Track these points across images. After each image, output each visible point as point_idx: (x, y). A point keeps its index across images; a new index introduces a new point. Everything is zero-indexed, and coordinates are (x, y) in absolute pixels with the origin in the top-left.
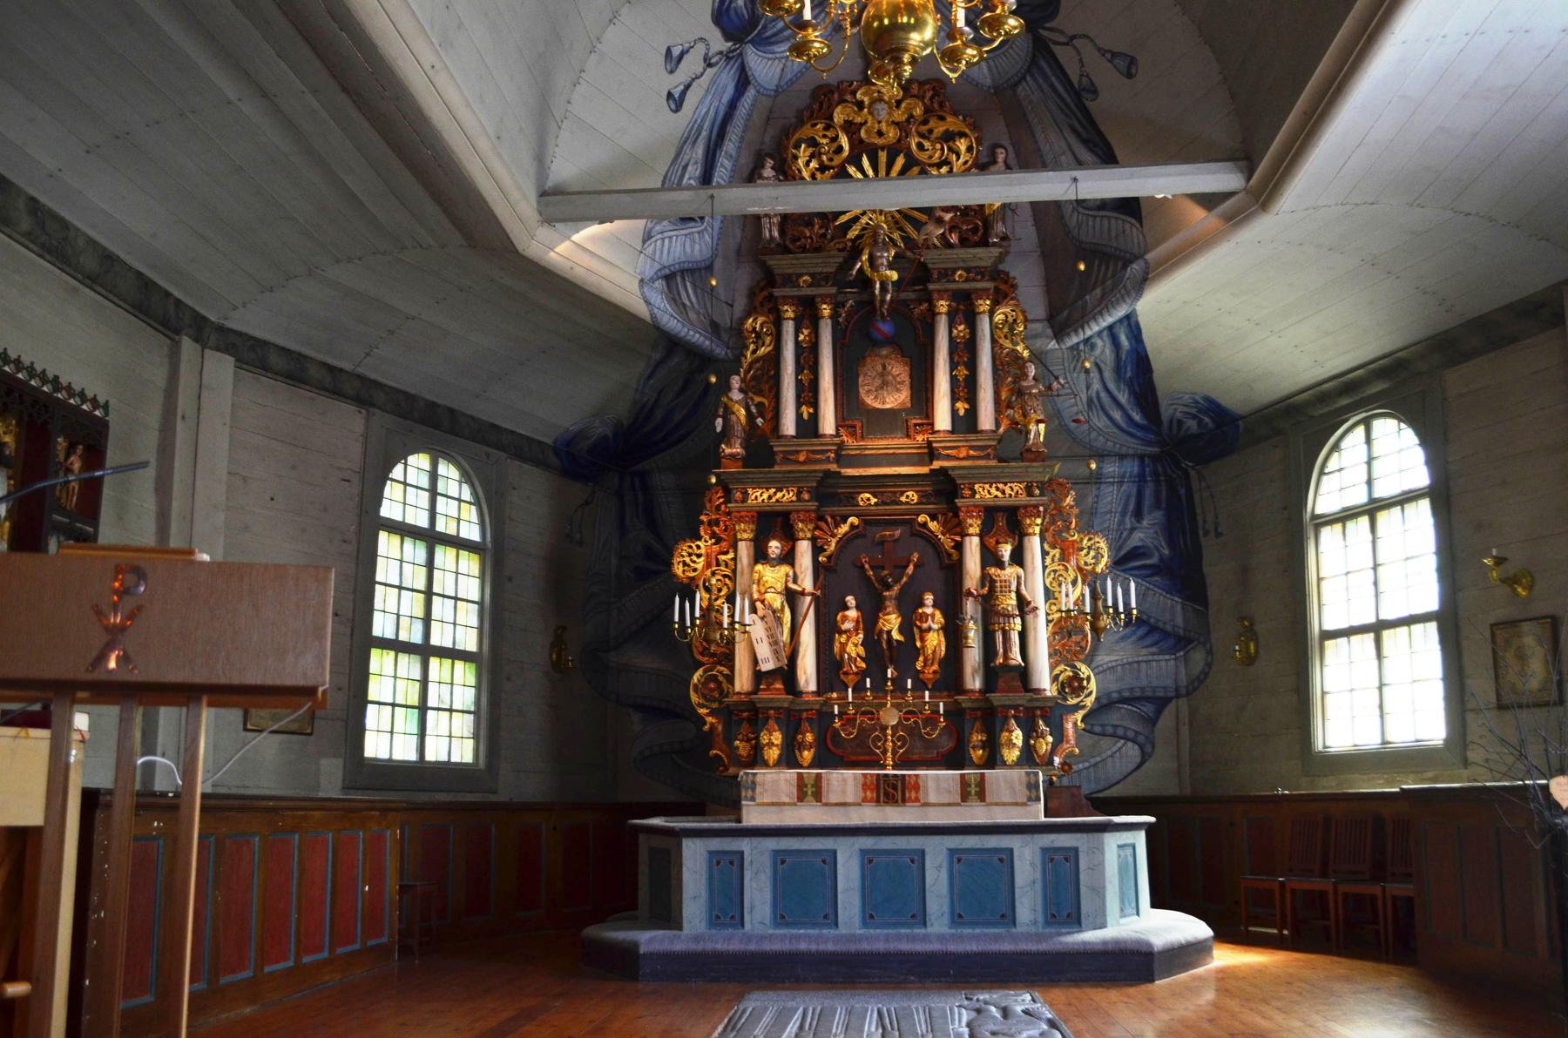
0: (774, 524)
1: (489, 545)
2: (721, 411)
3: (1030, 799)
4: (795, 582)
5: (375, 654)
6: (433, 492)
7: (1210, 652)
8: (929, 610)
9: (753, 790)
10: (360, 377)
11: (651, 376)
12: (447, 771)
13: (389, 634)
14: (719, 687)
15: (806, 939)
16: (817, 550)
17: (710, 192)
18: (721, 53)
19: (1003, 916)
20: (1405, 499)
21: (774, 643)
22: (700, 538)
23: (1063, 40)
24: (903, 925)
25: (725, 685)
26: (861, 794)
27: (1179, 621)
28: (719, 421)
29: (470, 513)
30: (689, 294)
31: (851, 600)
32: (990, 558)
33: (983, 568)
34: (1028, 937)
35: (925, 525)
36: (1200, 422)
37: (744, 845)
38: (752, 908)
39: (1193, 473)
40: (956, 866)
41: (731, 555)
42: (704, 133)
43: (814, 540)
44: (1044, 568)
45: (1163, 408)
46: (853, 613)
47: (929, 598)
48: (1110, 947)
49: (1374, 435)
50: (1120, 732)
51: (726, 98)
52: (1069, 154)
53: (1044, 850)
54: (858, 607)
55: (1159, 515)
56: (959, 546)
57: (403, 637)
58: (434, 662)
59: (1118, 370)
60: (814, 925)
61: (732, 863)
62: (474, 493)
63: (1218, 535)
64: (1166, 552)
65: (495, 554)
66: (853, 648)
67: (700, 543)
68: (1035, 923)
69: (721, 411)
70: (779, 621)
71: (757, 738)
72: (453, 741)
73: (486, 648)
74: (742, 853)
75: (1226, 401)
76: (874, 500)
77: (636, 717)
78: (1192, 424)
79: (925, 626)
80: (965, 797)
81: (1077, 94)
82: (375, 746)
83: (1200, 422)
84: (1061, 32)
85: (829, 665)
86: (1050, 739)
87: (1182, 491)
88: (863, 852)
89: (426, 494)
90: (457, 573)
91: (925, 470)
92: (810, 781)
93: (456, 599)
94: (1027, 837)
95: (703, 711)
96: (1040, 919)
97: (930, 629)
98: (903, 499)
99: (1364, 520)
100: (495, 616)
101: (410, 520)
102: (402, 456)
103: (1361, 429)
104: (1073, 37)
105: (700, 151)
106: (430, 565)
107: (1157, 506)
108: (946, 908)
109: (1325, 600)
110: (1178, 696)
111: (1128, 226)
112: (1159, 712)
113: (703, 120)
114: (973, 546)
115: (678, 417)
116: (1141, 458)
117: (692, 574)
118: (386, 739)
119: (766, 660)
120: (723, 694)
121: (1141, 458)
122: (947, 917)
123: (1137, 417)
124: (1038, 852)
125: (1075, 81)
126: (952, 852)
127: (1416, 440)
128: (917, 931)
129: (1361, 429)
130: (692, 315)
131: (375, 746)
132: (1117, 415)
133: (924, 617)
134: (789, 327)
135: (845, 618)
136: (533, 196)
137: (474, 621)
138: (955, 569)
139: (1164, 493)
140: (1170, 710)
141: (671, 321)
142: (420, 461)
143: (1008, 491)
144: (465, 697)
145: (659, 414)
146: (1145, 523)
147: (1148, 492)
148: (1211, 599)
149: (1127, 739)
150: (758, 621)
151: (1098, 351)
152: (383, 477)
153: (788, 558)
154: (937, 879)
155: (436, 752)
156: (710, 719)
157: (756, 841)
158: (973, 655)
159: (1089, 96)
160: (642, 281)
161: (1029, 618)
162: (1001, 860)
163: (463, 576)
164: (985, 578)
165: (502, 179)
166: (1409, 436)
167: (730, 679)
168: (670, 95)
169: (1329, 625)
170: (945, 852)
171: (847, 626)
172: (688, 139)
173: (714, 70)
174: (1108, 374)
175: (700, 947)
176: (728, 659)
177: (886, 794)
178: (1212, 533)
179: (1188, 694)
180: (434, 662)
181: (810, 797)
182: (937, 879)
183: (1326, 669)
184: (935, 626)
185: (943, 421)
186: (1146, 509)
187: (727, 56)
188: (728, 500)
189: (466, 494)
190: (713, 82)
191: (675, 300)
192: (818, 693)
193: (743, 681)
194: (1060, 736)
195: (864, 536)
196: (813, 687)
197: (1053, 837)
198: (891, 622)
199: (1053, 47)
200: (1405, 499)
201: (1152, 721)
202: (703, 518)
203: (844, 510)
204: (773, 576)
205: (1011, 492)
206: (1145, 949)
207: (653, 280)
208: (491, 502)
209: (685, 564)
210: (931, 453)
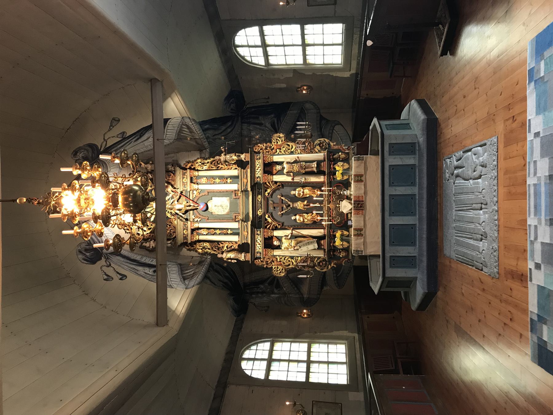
0: (268, 244)
1: (271, 339)
2: (230, 261)
3: (363, 160)
4: (288, 236)
5: (311, 380)
6: (254, 359)
7: (307, 102)
8: (297, 192)
9: (359, 251)
10: (217, 387)
11: (215, 284)
12: (351, 353)
13: (304, 375)
14: (323, 262)
15: (422, 234)
16: (276, 229)
17: (159, 266)
18: (106, 261)
19: (412, 169)
20: (262, 34)
21: (309, 243)
22: (272, 267)
23: (105, 143)
24: (415, 203)
25: (321, 260)
26: (360, 215)
27: (295, 112)
28: (233, 261)
29: (261, 346)
30: (190, 272)
31: (293, 218)
32: (280, 172)
33: (284, 174)
34: (420, 160)
35: (269, 193)
36: (232, 103)
37: (388, 255)
38: (409, 253)
39: (248, 106)
40: (395, 184)
41: (278, 257)
42: (134, 267)
43: (273, 230)
44: (283, 154)
45: (227, 115)
46: (298, 217)
47: (293, 192)
48: (425, 133)
49: (240, 44)
50: (331, 131)
51: (122, 259)
52: (144, 142)
53: (390, 154)
54: (295, 215)
55: (260, 117)
56: (276, 182)
57: (305, 370)
58: (312, 359)
59: (215, 129)
60: (415, 232)
61: (394, 260)
62: (253, 345)
63: (269, 98)
64: (273, 115)
65: (275, 337)
66: (308, 218)
67: (274, 267)
68: (414, 158)
69: (230, 261)
70: (301, 242)
71: (339, 249)
72: (338, 351)
73: (306, 340)
74: (390, 256)
75: (226, 95)
76: (260, 210)
77: (325, 288)
78: (233, 106)
79: (302, 194)
80: (361, 181)
81: (124, 139)
82: (343, 380)
83: (232, 103)
84: (103, 143)
85: (315, 225)
86: (340, 153)
87: (253, 110)
88: (390, 215)
89: (255, 362)
90: (328, 373)
91: (251, 193)
92: (356, 232)
93: (290, 351)
94: (385, 160)
95: (329, 267)
96: (413, 156)
97: (303, 192)
98: (260, 200)
99: (268, 49)
100: (295, 335)
101: (265, 368)
102: (242, 371)
103: (238, 49)
104: (104, 139)
105: (140, 268)
106: (279, 360)
107: (258, 118)
108: (409, 188)
109: (293, 63)
110: (320, 112)
111: (170, 123)
112: (325, 119)
113: (129, 267)
114: (276, 178)
115: (227, 274)
116: (242, 123)
117: (284, 270)
118: (339, 376)
119: (314, 246)
120: (324, 260)
121: (242, 123)
122: (412, 187)
123: (230, 123)
124: (390, 157)
125: (120, 139)
126: (390, 185)
127: (243, 30)
128: (417, 197)
129: (238, 49)
130: (197, 270)
131: (343, 380)
132: (229, 130)
133: (299, 194)
134: (201, 238)
135: (299, 220)
136: (159, 329)
137: (297, 344)
138: (283, 184)
139: (253, 116)
140: (324, 115)
141: (198, 278)
142: (245, 365)
143: (258, 166)
144: (323, 347)
145: (226, 281)
146: (263, 122)
147: (252, 120)
148: (289, 101)
149: (333, 129)
150: (302, 248)
151: (210, 135)
152: (250, 378)
153: (279, 239)
154: (400, 190)
155: (343, 358)
156: (332, 265)
157: (386, 252)
158: (313, 179)
159: (125, 134)
160: (186, 288)
161: (301, 160)
162: (393, 169)
163: (282, 349)
164: (288, 174)
165: (152, 342)
166: (241, 33)
167: (319, 258)
168: (121, 279)
169: (341, 47)
170: (391, 188)
171: (302, 220)
172: (136, 272)
173: (111, 263)
174: (216, 133)
175: (425, 271)
176: (313, 258)
177: (361, 207)
178: (268, 100)
179: (319, 109)
180: (312, 359)
181: (362, 232)
182: (400, 190)
183: (316, 63)
184: (302, 190)
185: (235, 187)
186: (259, 122)
187: (107, 259)
188: (260, 258)
189: (254, 347)
190: (116, 264)
191: (192, 277)
192: (324, 229)
193: (321, 254)
194: (338, 151)
195: (272, 213)
196: (322, 231)
197: (385, 152)
198: (300, 205)
199: (107, 146)
200: (262, 34)
201: (328, 121)
202: (265, 266)
203: (263, 220)
204: (285, 243)
205: (259, 164)
206: (426, 121)
207: (185, 284)
208: (256, 338)
209: (280, 272)
210: (245, 191)
